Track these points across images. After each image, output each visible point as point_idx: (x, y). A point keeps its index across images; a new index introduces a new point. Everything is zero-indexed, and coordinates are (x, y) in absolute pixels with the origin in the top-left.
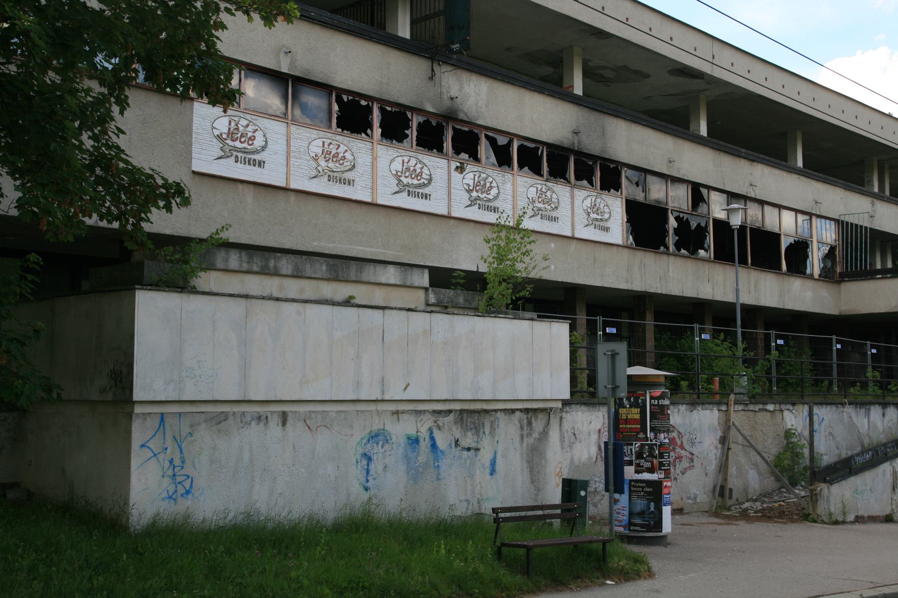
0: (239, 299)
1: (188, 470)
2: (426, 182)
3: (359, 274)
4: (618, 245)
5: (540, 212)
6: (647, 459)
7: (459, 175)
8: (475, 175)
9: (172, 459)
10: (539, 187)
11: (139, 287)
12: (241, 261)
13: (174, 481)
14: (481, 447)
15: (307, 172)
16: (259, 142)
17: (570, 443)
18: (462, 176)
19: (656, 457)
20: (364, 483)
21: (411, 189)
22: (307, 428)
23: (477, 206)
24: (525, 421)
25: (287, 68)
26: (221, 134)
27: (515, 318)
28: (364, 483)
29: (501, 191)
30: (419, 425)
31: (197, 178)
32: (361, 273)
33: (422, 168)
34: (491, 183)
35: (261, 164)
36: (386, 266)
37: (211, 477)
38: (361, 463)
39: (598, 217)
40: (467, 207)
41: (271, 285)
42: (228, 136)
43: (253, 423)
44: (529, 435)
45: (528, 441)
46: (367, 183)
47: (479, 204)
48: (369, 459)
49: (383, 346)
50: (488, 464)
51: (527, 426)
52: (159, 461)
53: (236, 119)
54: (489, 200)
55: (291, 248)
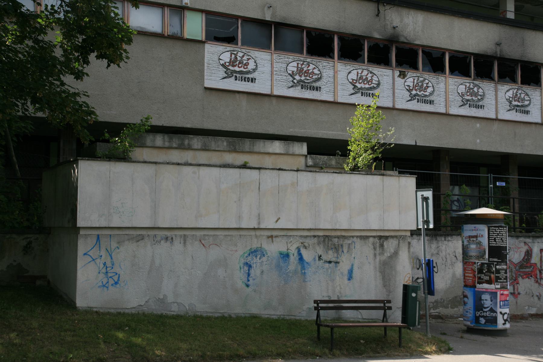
0: (150, 165)
1: (116, 269)
2: (375, 86)
3: (252, 147)
4: (536, 124)
5: (469, 102)
6: (486, 274)
7: (402, 80)
8: (414, 79)
9: (105, 263)
10: (468, 85)
11: (80, 158)
12: (164, 141)
13: (107, 276)
14: (340, 261)
15: (286, 84)
16: (251, 66)
17: (452, 262)
18: (404, 80)
19: (493, 273)
20: (246, 282)
21: (364, 91)
22: (202, 245)
23: (416, 100)
24: (378, 245)
25: (270, 18)
26: (225, 63)
27: (367, 174)
28: (246, 282)
29: (436, 89)
30: (289, 245)
31: (208, 92)
32: (253, 146)
33: (372, 76)
34: (427, 84)
35: (253, 80)
36: (272, 142)
37: (132, 274)
38: (243, 268)
39: (519, 104)
40: (408, 101)
41: (188, 156)
42: (230, 64)
43: (162, 242)
44: (382, 254)
45: (380, 258)
46: (330, 89)
47: (418, 99)
48: (250, 266)
49: (259, 193)
50: (346, 272)
51: (380, 248)
52: (96, 263)
53: (235, 52)
54: (426, 96)
55: (273, 133)
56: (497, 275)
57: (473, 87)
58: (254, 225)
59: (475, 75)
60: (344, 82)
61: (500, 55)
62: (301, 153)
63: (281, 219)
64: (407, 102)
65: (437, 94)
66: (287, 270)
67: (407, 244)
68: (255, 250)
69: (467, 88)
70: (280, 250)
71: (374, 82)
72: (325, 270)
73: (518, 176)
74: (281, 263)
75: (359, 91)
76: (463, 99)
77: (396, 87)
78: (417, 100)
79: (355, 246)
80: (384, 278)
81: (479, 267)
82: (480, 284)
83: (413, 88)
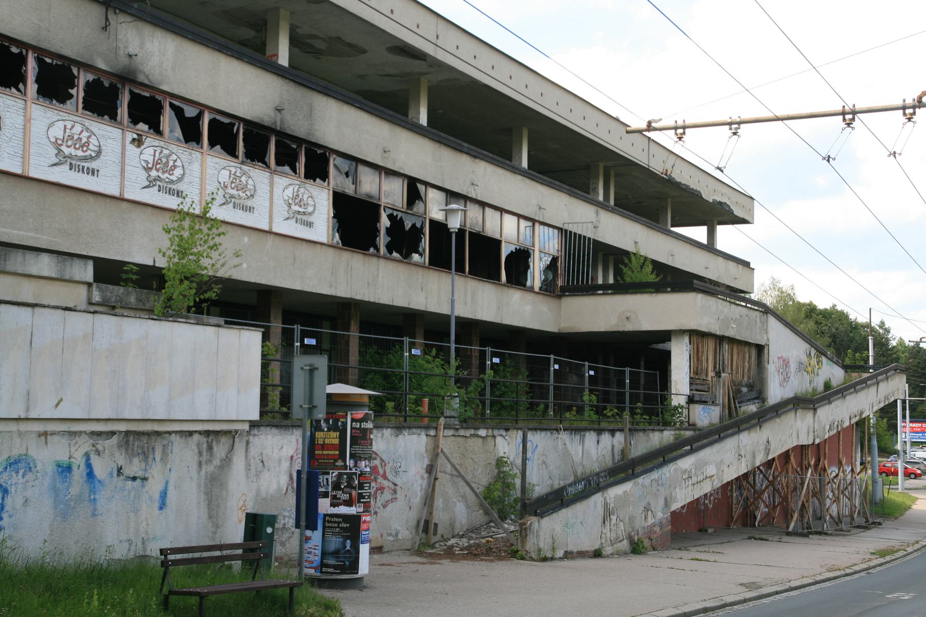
2: (93, 154)
4: (322, 244)
5: (233, 200)
6: (345, 490)
7: (136, 149)
8: (155, 151)
17: (256, 471)
18: (139, 150)
19: (355, 488)
21: (74, 162)
23: (156, 188)
24: (205, 446)
27: (197, 324)
29: (187, 171)
30: (73, 449)
32: (5, 261)
33: (89, 137)
34: (175, 161)
36: (38, 255)
44: (209, 461)
45: (206, 469)
47: (159, 186)
49: (31, 352)
50: (157, 496)
54: (172, 182)
56: (359, 491)
57: (239, 175)
58: (18, 411)
59: (244, 155)
60: (42, 142)
61: (281, 128)
62: (84, 280)
63: (64, 400)
64: (144, 190)
65: (188, 181)
66: (67, 496)
67: (244, 443)
68: (15, 461)
69: (232, 176)
70: (58, 459)
71: (91, 147)
72: (126, 493)
73: (360, 333)
74: (58, 484)
75: (66, 161)
76: (226, 193)
77: (127, 161)
78: (157, 187)
79: (172, 450)
80: (209, 504)
81: (334, 479)
82: (334, 507)
83: (153, 165)
